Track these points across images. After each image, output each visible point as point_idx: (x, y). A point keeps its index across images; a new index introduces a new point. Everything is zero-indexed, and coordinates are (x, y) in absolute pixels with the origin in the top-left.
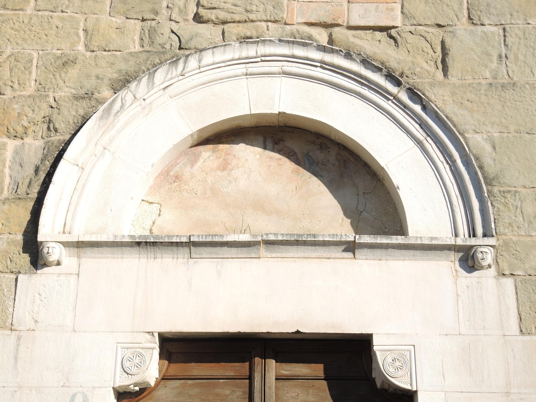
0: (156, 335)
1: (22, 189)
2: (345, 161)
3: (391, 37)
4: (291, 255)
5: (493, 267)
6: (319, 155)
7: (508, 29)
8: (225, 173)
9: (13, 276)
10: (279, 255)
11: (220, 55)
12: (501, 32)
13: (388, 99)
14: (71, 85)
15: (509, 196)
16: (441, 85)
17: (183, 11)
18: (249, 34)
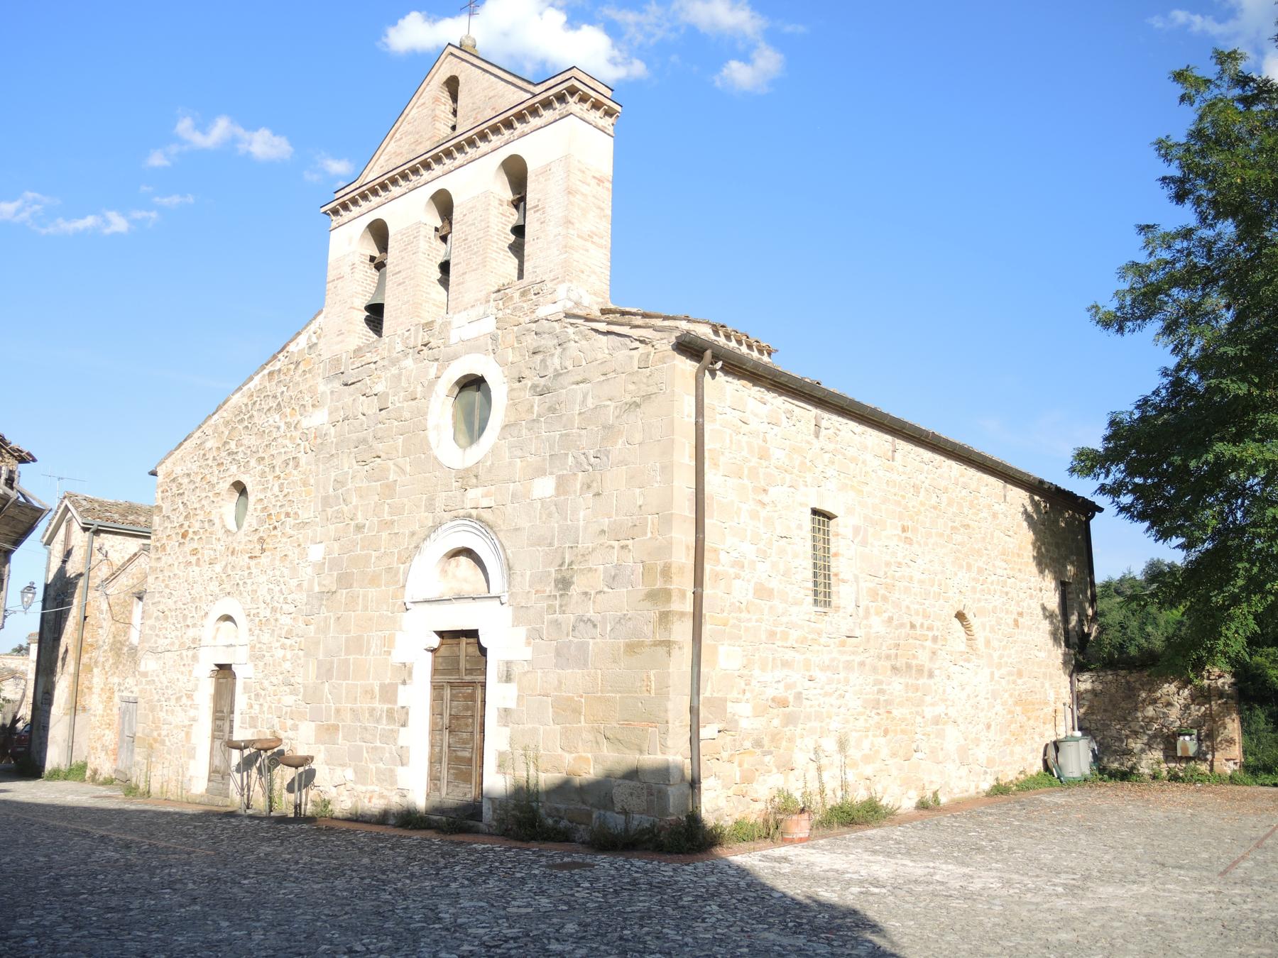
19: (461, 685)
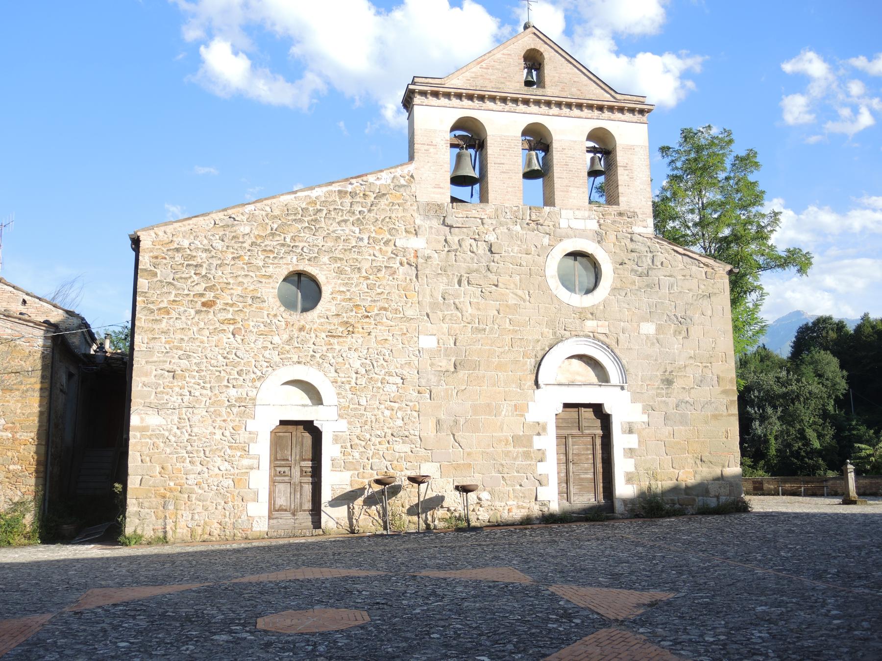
6: (590, 362)
17: (562, 328)
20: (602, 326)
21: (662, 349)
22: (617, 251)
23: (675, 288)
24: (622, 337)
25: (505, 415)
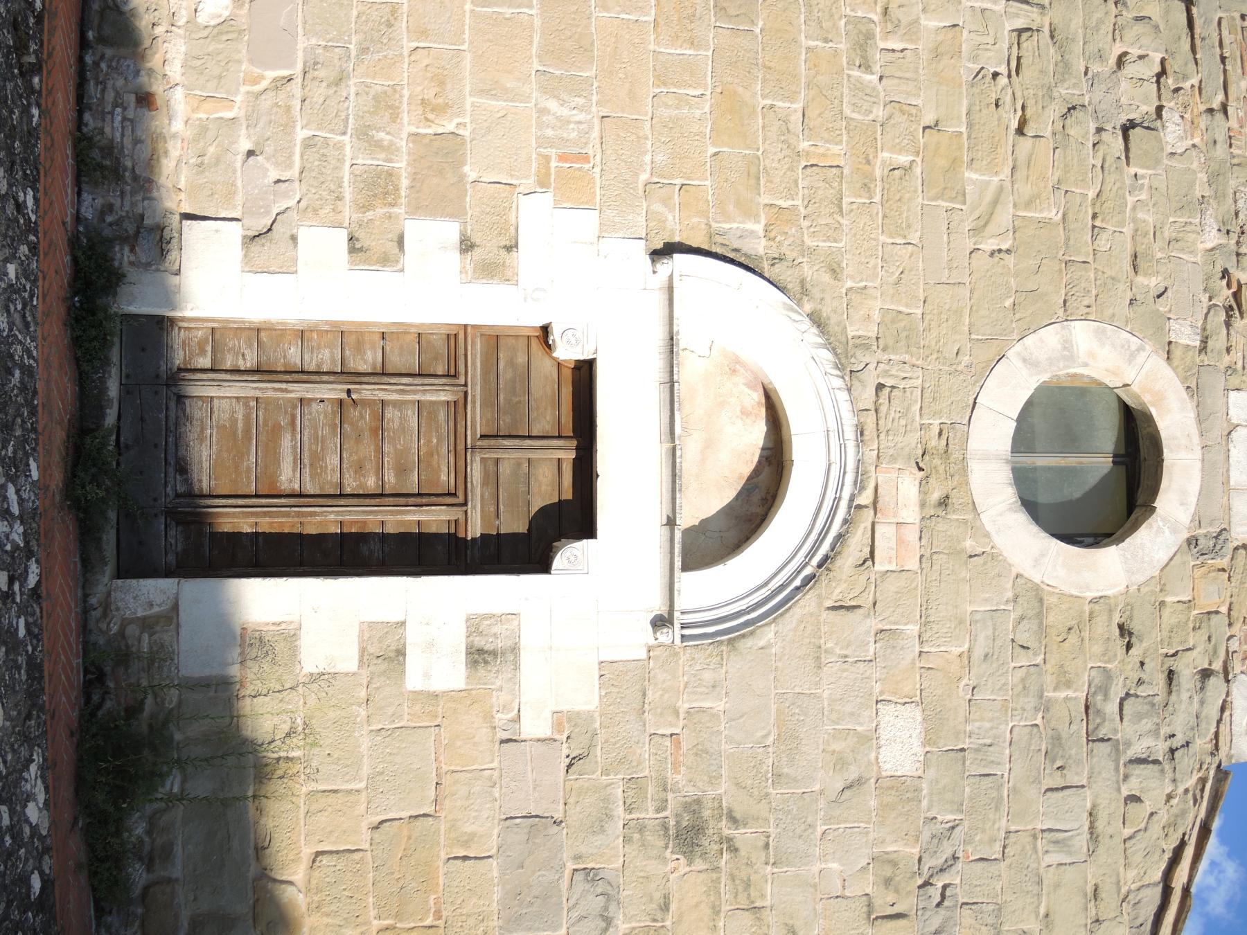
0: (594, 356)
1: (719, 239)
2: (750, 520)
3: (865, 561)
4: (664, 470)
5: (656, 642)
6: (756, 498)
7: (871, 664)
8: (739, 413)
9: (643, 236)
10: (664, 460)
11: (845, 408)
12: (869, 658)
13: (806, 557)
14: (815, 276)
15: (719, 658)
16: (820, 604)
17: (886, 373)
18: (866, 433)
19: (461, 447)
20: (900, 541)
21: (822, 803)
22: (1166, 612)
23: (1054, 858)
24: (863, 625)
25: (543, 111)
